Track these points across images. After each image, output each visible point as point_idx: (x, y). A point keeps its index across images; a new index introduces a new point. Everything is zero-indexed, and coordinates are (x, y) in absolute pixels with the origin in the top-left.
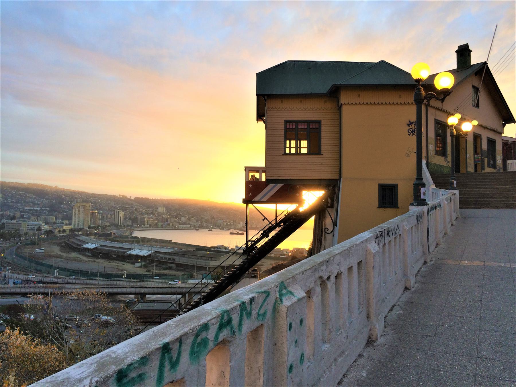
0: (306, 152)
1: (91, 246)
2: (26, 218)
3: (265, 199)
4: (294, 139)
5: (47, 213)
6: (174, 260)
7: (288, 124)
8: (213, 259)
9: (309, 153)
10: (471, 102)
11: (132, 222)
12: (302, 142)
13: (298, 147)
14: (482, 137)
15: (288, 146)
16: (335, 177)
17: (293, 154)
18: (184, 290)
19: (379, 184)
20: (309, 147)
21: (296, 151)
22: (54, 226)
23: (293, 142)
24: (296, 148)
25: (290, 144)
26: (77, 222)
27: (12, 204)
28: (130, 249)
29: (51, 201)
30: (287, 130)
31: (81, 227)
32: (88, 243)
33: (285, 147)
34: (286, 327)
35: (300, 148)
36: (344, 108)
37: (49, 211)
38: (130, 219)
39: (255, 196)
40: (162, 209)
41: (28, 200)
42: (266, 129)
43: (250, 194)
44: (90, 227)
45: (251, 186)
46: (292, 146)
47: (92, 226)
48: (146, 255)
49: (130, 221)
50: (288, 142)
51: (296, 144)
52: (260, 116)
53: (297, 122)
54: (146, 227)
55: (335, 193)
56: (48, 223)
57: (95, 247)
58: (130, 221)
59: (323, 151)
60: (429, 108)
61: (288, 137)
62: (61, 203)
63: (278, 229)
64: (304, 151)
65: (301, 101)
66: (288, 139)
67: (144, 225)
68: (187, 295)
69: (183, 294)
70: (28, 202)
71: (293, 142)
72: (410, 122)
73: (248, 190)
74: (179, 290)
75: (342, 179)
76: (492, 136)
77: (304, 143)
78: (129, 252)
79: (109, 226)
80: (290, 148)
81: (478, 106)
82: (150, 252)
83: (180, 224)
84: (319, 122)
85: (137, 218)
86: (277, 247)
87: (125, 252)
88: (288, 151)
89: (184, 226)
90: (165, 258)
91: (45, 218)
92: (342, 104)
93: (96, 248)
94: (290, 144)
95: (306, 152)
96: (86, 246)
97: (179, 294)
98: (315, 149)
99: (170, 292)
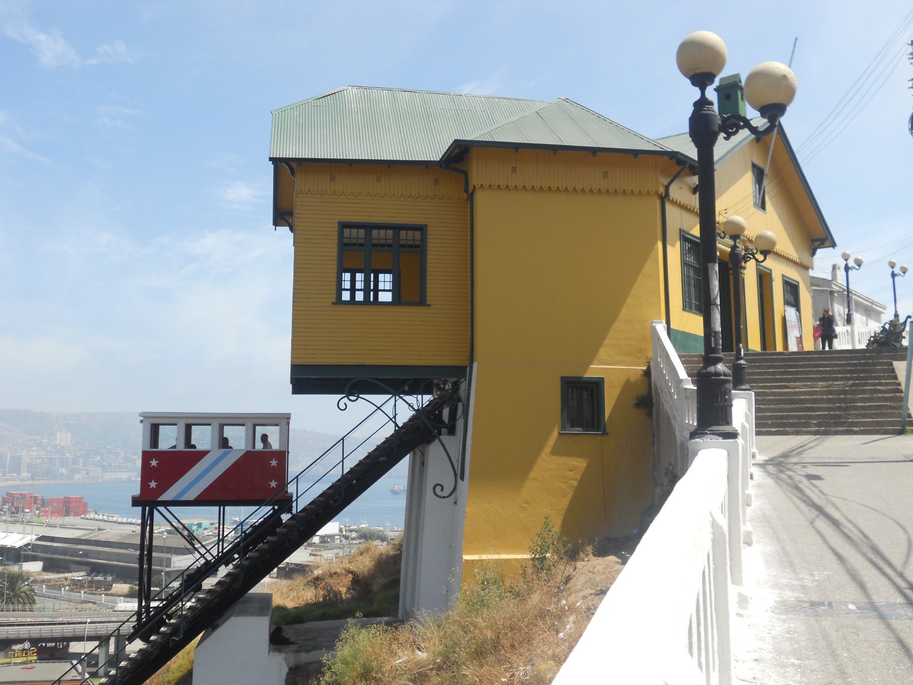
0: (390, 300)
3: (191, 495)
4: (360, 271)
7: (347, 231)
9: (398, 300)
10: (751, 200)
12: (381, 276)
13: (372, 289)
14: (773, 276)
16: (465, 363)
17: (359, 303)
18: (103, 629)
19: (563, 378)
20: (396, 290)
21: (367, 296)
23: (359, 277)
24: (366, 290)
25: (353, 281)
30: (345, 246)
33: (340, 290)
35: (376, 291)
36: (481, 199)
39: (165, 486)
40: (63, 439)
43: (153, 484)
45: (154, 463)
46: (381, 287)
50: (347, 276)
51: (367, 281)
53: (369, 227)
55: (459, 400)
59: (430, 297)
60: (669, 208)
63: (223, 571)
64: (386, 297)
65: (379, 180)
66: (346, 271)
67: (19, 474)
69: (103, 640)
72: (699, 65)
73: (147, 473)
74: (88, 629)
75: (475, 365)
76: (794, 274)
77: (386, 280)
80: (353, 290)
81: (763, 206)
86: (252, 591)
88: (346, 296)
94: (353, 281)
95: (390, 300)
97: (91, 638)
98: (410, 293)
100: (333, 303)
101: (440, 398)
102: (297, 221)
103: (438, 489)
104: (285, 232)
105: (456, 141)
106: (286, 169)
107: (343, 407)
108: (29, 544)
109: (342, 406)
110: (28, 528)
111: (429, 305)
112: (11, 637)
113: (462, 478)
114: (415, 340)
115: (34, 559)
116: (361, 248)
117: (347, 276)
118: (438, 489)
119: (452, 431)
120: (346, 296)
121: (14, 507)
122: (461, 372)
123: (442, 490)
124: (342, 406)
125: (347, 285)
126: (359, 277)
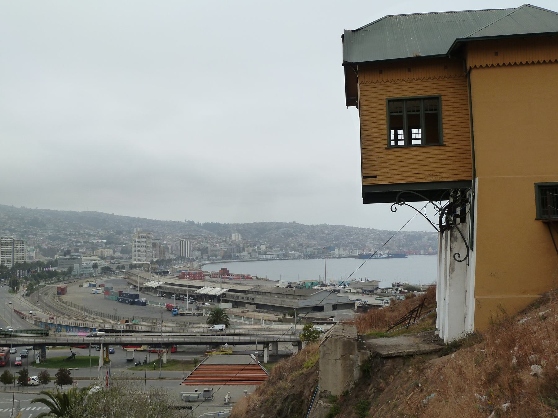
1: (153, 284)
2: (81, 252)
5: (104, 246)
6: (137, 297)
8: (302, 298)
11: (202, 254)
13: (408, 138)
15: (393, 137)
18: (265, 339)
22: (112, 261)
23: (400, 132)
26: (137, 256)
27: (66, 237)
28: (199, 287)
29: (108, 232)
31: (143, 261)
32: (150, 281)
34: (206, 389)
37: (106, 244)
38: (199, 249)
40: (236, 237)
41: (82, 232)
42: (360, 116)
44: (152, 262)
46: (399, 137)
47: (155, 259)
48: (218, 294)
49: (199, 252)
50: (392, 132)
52: (351, 100)
54: (218, 260)
56: (105, 258)
57: (158, 285)
58: (199, 252)
61: (395, 124)
62: (120, 233)
67: (216, 257)
68: (270, 344)
69: (266, 344)
70: (82, 234)
71: (400, 132)
74: (259, 339)
75: (477, 179)
78: (199, 291)
79: (175, 260)
80: (396, 140)
82: (223, 291)
83: (260, 253)
84: (437, 98)
85: (207, 248)
87: (193, 291)
89: (265, 257)
90: (242, 298)
91: (102, 252)
92: (470, 68)
93: (160, 286)
96: (148, 284)
97: (259, 343)
98: (432, 138)
99: (204, 341)
100: (386, 148)
101: (455, 201)
102: (360, 100)
103: (457, 256)
104: (354, 110)
105: (457, 39)
106: (353, 71)
107: (394, 210)
108: (224, 294)
109: (394, 209)
110: (223, 285)
111: (445, 145)
112: (219, 341)
113: (472, 249)
114: (437, 166)
115: (227, 301)
116: (401, 115)
117: (392, 132)
118: (457, 256)
119: (463, 221)
120: (393, 143)
121: (6, 275)
122: (466, 186)
123: (459, 257)
124: (394, 209)
125: (393, 137)
126: (399, 132)
